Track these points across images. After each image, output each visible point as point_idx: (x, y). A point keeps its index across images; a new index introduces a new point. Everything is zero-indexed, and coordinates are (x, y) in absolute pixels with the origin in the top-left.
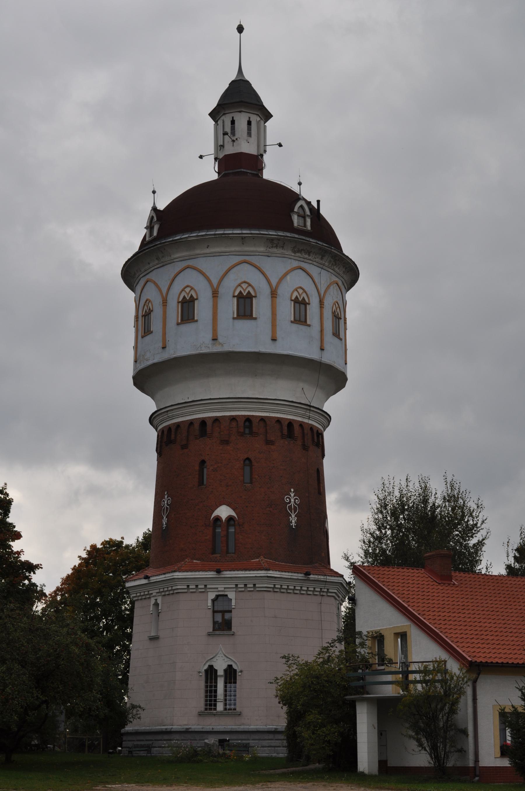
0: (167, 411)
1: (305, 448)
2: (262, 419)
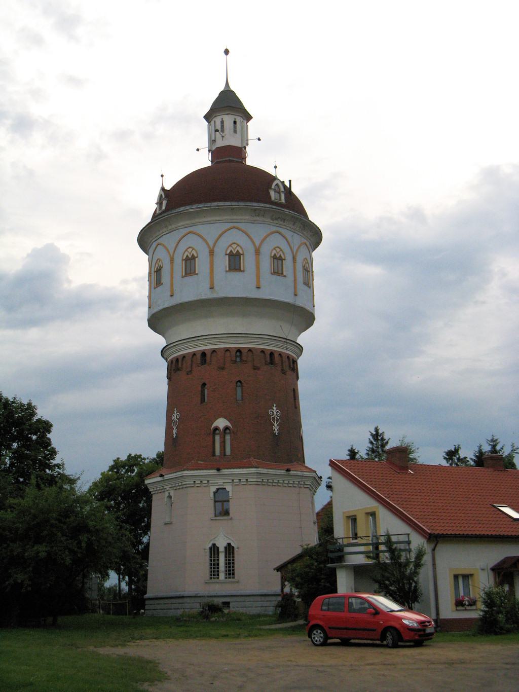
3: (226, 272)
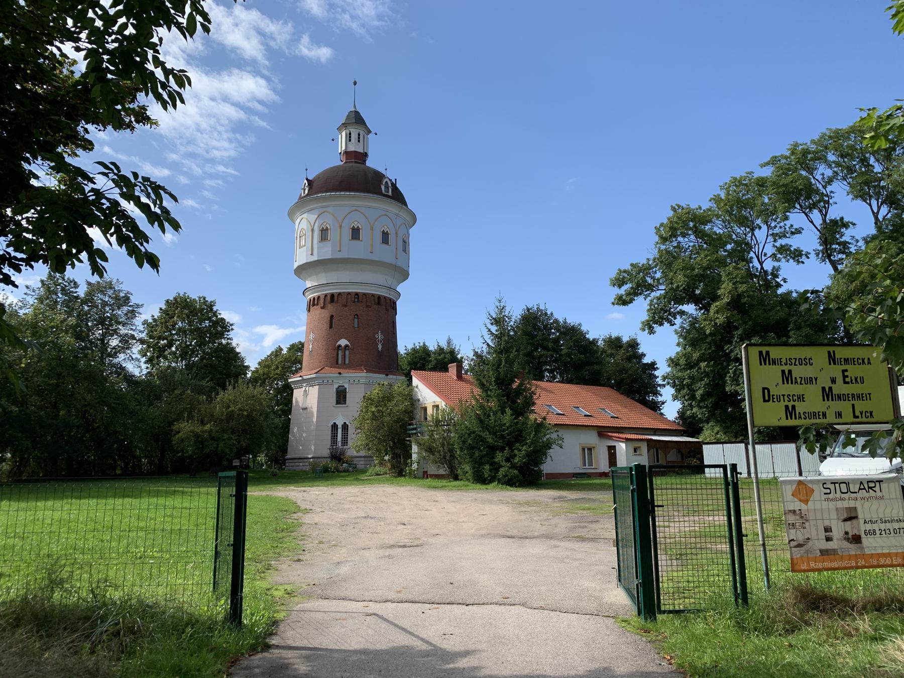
1: (387, 310)
2: (364, 294)
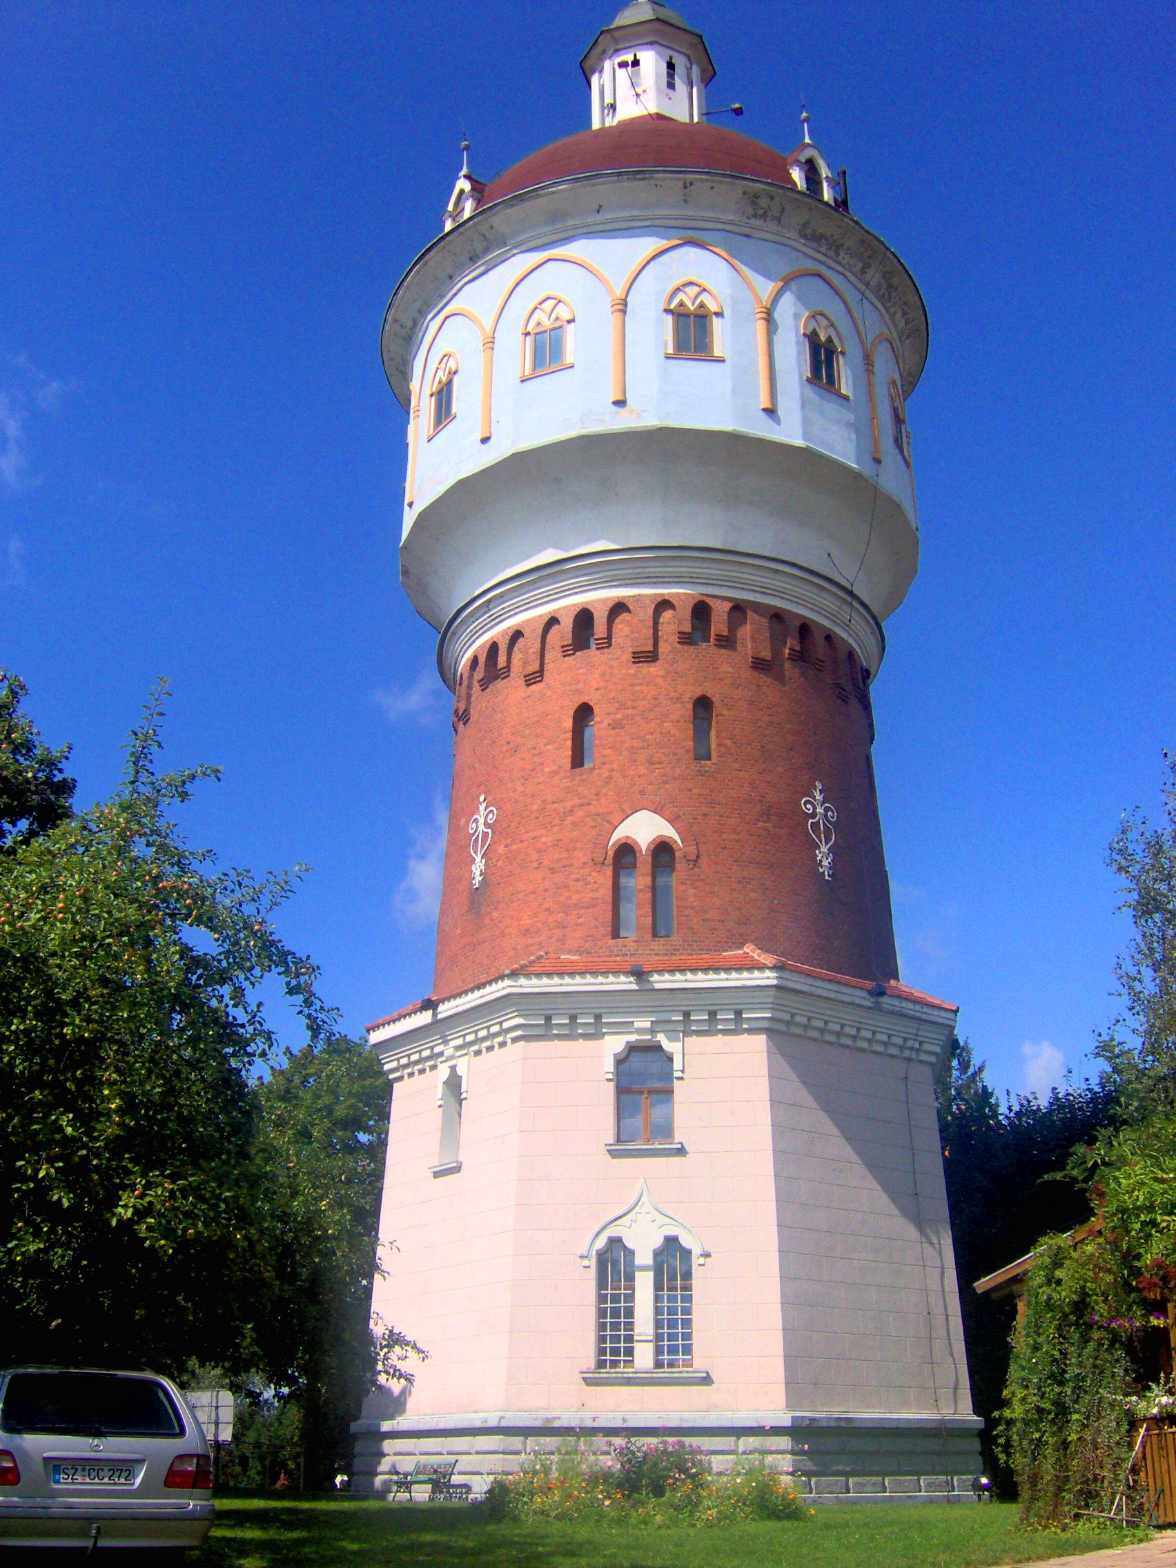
0: (489, 601)
3: (668, 357)
